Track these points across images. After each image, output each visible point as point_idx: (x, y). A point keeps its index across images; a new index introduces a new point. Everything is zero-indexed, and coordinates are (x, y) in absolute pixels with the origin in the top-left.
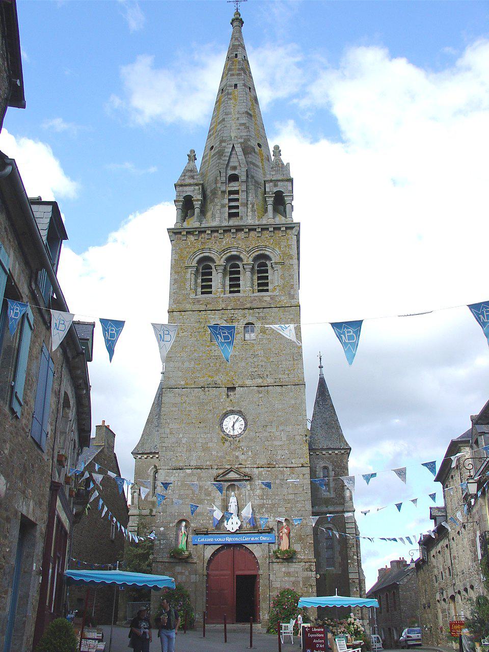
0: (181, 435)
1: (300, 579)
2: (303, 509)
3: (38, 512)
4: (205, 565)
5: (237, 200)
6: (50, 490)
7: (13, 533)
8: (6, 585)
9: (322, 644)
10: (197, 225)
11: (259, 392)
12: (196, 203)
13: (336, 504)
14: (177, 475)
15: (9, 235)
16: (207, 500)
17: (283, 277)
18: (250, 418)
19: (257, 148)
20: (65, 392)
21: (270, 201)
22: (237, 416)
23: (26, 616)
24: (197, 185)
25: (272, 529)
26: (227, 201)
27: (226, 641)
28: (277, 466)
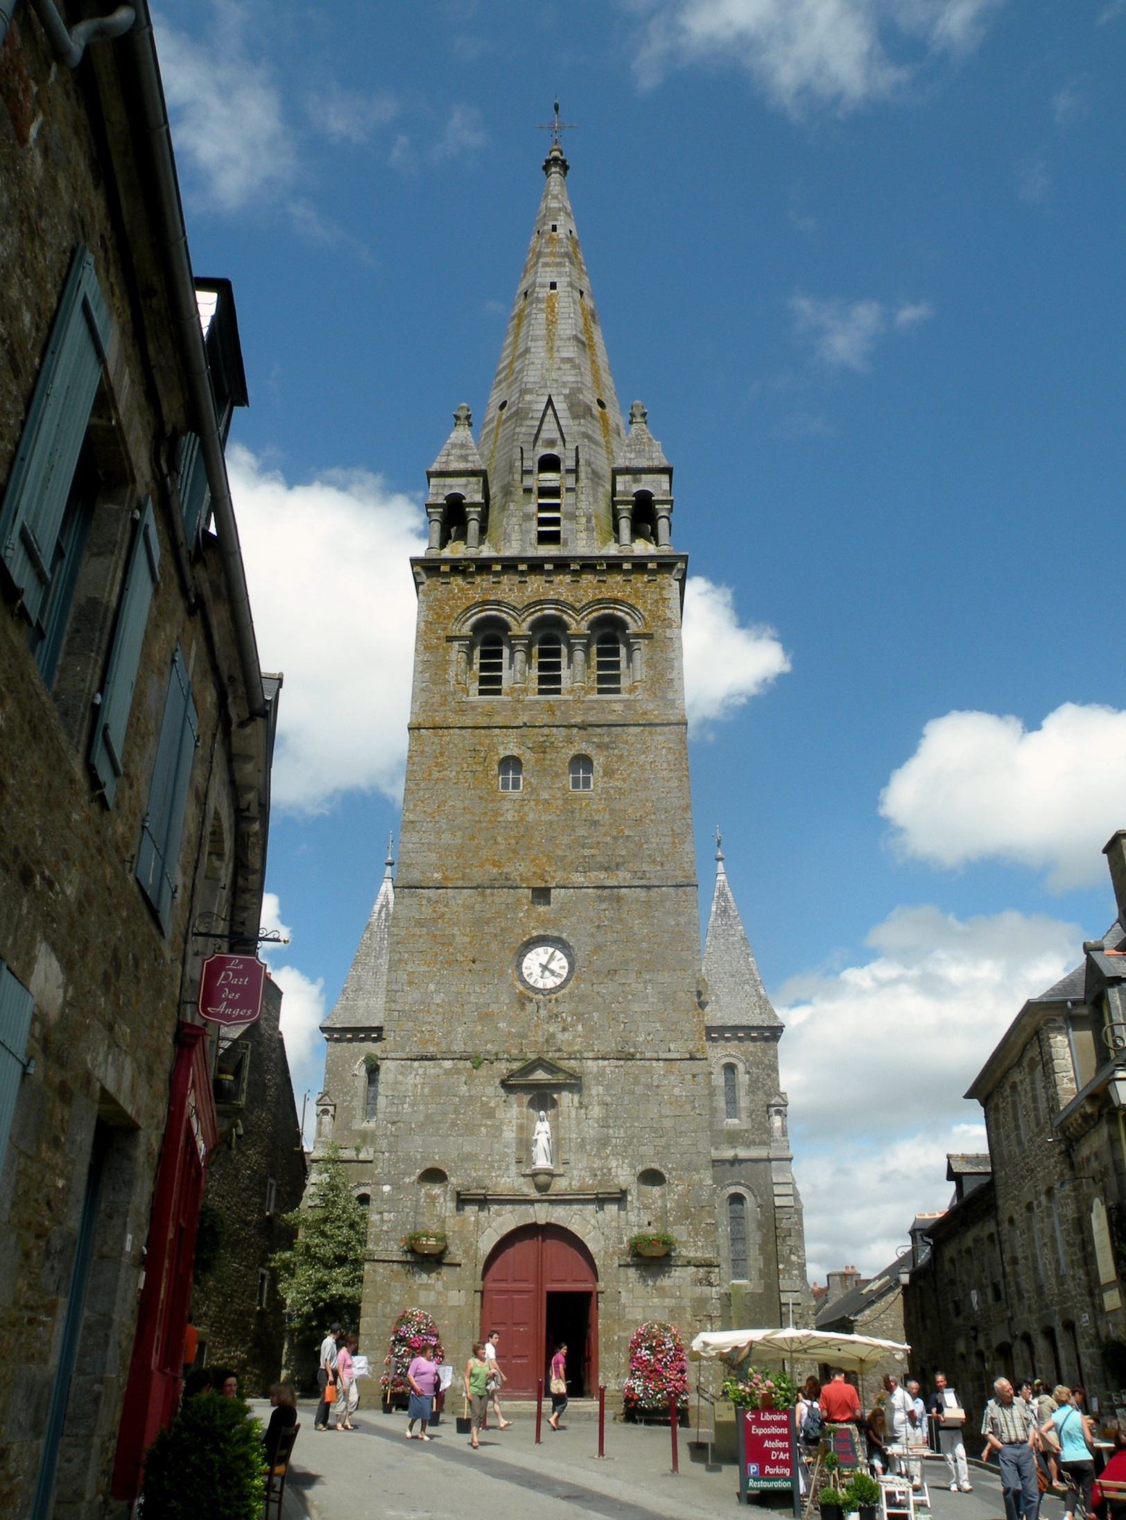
0: (432, 987)
1: (686, 1302)
2: (693, 1149)
3: (143, 1093)
4: (480, 1267)
5: (556, 507)
7: (78, 1138)
8: (52, 1288)
9: (784, 1450)
10: (472, 552)
11: (601, 899)
12: (472, 509)
14: (421, 1071)
15: (112, 270)
16: (486, 1126)
17: (650, 664)
18: (580, 954)
19: (596, 409)
20: (216, 808)
21: (625, 511)
22: (552, 950)
23: (101, 1381)
24: (473, 473)
25: (624, 1193)
26: (534, 508)
27: (538, 1440)
28: (638, 1056)
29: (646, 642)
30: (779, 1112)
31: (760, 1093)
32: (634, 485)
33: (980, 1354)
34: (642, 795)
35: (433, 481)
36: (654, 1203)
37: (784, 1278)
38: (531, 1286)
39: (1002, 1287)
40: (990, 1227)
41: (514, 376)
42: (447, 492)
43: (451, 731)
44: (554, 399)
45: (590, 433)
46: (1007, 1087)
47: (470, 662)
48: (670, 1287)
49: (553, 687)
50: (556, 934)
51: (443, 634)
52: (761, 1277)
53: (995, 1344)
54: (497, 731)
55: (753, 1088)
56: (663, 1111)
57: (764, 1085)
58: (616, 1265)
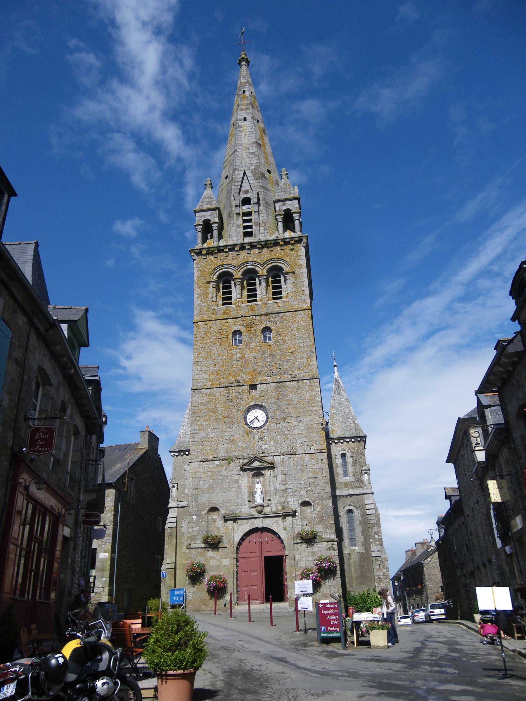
0: (209, 430)
2: (323, 491)
4: (235, 548)
5: (250, 221)
9: (336, 620)
10: (216, 244)
17: (295, 285)
21: (280, 219)
24: (214, 209)
25: (295, 512)
26: (241, 222)
29: (292, 275)
30: (366, 473)
31: (358, 465)
32: (283, 207)
33: (465, 575)
34: (293, 341)
35: (197, 214)
36: (308, 516)
37: (373, 546)
38: (257, 554)
39: (469, 545)
40: (462, 519)
41: (231, 163)
42: (203, 219)
43: (211, 322)
44: (246, 172)
45: (264, 185)
46: (460, 457)
47: (218, 290)
48: (316, 551)
49: (254, 299)
50: (260, 404)
51: (205, 281)
52: (363, 546)
53: (469, 571)
54: (230, 320)
55: (354, 464)
56: (309, 476)
57: (359, 462)
58: (293, 543)
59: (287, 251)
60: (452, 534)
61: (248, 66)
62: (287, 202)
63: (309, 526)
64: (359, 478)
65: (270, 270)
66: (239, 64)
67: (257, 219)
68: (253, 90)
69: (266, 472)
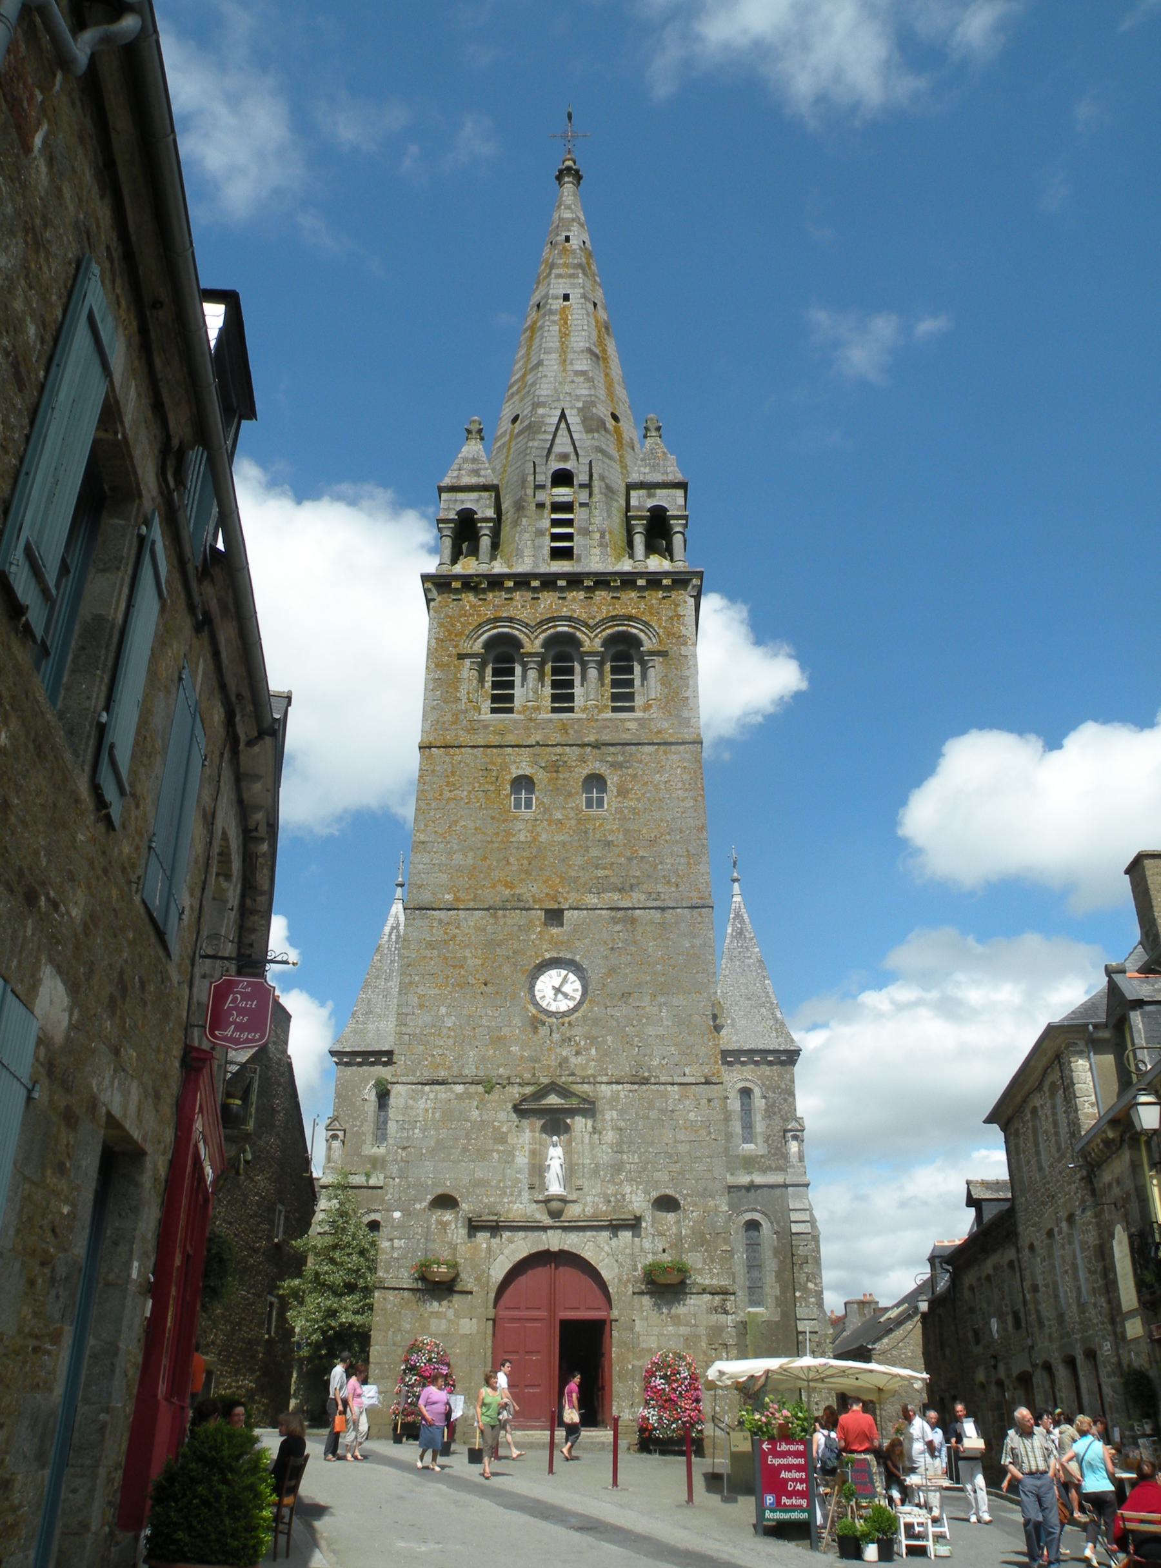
0: (443, 1010)
1: (702, 1331)
3: (150, 1117)
4: (492, 1295)
5: (569, 523)
6: (181, 1066)
7: (84, 1164)
9: (801, 1481)
10: (483, 568)
11: (615, 921)
13: (770, 1169)
14: (432, 1096)
15: (118, 282)
16: (498, 1151)
17: (665, 682)
18: (594, 977)
19: (610, 423)
20: (223, 828)
21: (639, 527)
23: (107, 1410)
24: (485, 488)
25: (638, 1219)
26: (546, 523)
30: (795, 1138)
32: (648, 500)
33: (1000, 1384)
35: (444, 496)
36: (669, 1229)
37: (801, 1306)
38: (543, 1314)
39: (1022, 1315)
42: (459, 507)
43: (463, 750)
44: (567, 412)
45: (604, 447)
48: (685, 1314)
49: (566, 705)
50: (569, 956)
52: (778, 1305)
53: (1015, 1372)
54: (509, 750)
55: (770, 1112)
57: (780, 1110)
58: (630, 1292)
59: (654, 601)
60: (972, 1288)
61: (579, 184)
62: (658, 491)
63: (670, 1255)
64: (777, 1148)
65: (610, 641)
66: (559, 178)
67: (584, 520)
68: (586, 238)
69: (579, 1124)
